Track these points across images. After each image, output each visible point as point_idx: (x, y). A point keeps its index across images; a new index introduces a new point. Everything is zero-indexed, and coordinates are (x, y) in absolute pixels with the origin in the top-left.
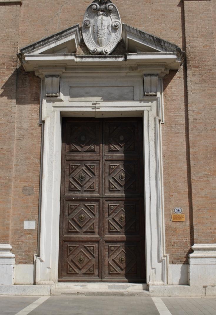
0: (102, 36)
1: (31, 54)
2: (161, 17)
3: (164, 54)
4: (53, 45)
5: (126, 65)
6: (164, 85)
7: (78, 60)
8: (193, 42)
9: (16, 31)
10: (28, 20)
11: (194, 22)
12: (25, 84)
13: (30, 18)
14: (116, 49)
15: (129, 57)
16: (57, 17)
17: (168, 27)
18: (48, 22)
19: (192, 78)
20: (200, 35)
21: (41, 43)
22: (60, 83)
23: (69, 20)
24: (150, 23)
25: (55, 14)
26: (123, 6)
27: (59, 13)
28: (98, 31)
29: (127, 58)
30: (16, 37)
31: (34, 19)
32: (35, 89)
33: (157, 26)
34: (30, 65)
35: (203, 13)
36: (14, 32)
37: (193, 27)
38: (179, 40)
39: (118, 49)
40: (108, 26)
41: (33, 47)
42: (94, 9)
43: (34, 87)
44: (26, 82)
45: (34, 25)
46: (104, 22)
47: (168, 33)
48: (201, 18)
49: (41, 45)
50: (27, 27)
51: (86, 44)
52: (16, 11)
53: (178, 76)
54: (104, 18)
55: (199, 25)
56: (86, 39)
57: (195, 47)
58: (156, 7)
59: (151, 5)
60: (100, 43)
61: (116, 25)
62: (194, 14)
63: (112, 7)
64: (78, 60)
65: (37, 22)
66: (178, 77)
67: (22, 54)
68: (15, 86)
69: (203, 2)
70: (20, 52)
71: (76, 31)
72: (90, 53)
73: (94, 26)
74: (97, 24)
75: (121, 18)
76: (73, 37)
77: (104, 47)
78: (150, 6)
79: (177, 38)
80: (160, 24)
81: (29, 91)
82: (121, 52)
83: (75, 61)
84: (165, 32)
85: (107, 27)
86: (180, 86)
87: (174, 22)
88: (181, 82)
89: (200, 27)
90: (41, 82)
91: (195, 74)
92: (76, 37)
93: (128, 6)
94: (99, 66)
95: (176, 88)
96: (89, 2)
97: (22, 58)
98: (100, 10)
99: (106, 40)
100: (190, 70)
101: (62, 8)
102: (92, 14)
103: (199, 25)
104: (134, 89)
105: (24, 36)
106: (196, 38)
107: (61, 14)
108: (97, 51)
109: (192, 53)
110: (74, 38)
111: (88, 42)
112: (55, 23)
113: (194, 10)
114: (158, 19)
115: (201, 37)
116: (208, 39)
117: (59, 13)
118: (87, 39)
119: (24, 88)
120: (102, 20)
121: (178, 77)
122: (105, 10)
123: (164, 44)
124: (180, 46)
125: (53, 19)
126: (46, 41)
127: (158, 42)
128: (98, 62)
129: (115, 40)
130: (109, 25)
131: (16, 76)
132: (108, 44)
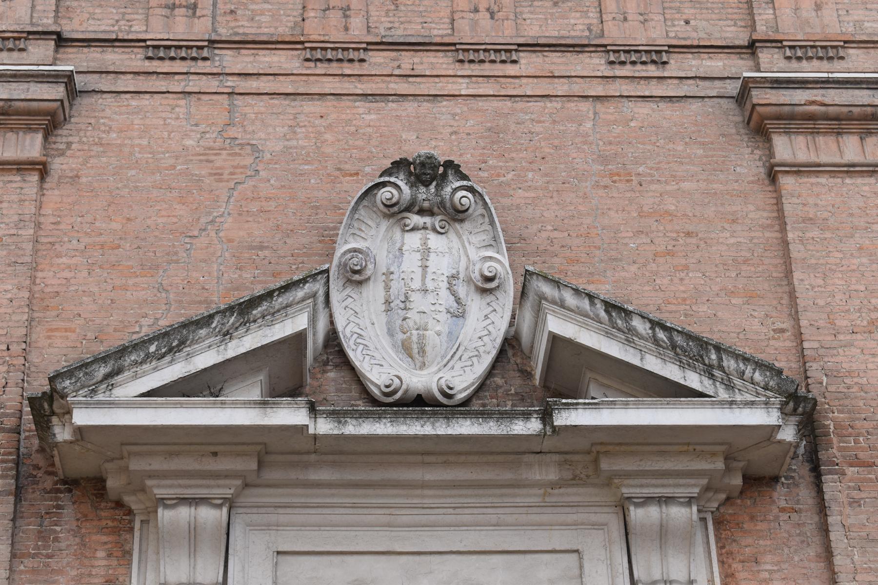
1: (100, 397)
2: (681, 242)
3: (722, 404)
4: (205, 358)
6: (723, 547)
7: (324, 427)
8: (835, 352)
9: (15, 291)
10: (75, 242)
11: (834, 267)
12: (56, 539)
13: (86, 233)
14: (488, 382)
15: (565, 418)
16: (213, 234)
17: (716, 288)
18: (168, 254)
19: (848, 516)
20: (865, 323)
21: (152, 349)
22: (228, 534)
23: (267, 247)
24: (633, 268)
25: (203, 220)
26: (511, 192)
27: (222, 216)
28: (407, 297)
30: (14, 318)
31: (102, 239)
32: (104, 563)
33: (666, 281)
34: (89, 446)
35: (866, 228)
36: (9, 296)
37: (830, 288)
38: (772, 342)
39: (499, 380)
41: (117, 360)
42: (388, 203)
43: (101, 554)
44: (58, 528)
45: (101, 267)
46: (433, 262)
47: (719, 314)
48: (860, 248)
49: (148, 357)
50: (67, 274)
51: (351, 354)
52: (22, 201)
53: (783, 504)
54: (434, 241)
55: (854, 281)
56: (349, 335)
57: (850, 373)
58: (657, 200)
59: (633, 190)
60: (416, 351)
61: (489, 275)
62: (828, 235)
63: (470, 195)
64: (324, 427)
65: (116, 251)
66: (783, 510)
67: (56, 396)
68: (658, 541)
69: (864, 185)
70: (47, 388)
71: (314, 295)
72: (374, 401)
74: (404, 267)
76: (298, 322)
77: (434, 368)
78: (628, 195)
79: (763, 337)
80: (683, 275)
81: (74, 573)
82: (513, 392)
83: (311, 431)
84: (705, 308)
85: (445, 279)
86: (796, 551)
87: (744, 267)
88: (799, 535)
89: (862, 288)
90: (132, 529)
91: (863, 495)
93: (532, 194)
95: (778, 563)
96: (357, 174)
97: (53, 413)
98: (417, 208)
99: (444, 337)
100: (836, 477)
101: (235, 193)
102: (378, 225)
103: (854, 281)
104: (581, 567)
105: (54, 313)
106: (849, 337)
107: (230, 220)
108: (404, 387)
109: (837, 403)
111: (361, 347)
112: (205, 261)
113: (826, 215)
114: (670, 253)
115: (870, 332)
116: (572, 222)
117: (222, 216)
118: (353, 333)
119: (49, 556)
120: (426, 252)
121: (783, 510)
122: (436, 209)
123: (720, 359)
124: (787, 364)
125: (194, 242)
126: (174, 340)
127: (695, 349)
128: (415, 437)
130: (454, 272)
131: (12, 499)
132: (452, 357)
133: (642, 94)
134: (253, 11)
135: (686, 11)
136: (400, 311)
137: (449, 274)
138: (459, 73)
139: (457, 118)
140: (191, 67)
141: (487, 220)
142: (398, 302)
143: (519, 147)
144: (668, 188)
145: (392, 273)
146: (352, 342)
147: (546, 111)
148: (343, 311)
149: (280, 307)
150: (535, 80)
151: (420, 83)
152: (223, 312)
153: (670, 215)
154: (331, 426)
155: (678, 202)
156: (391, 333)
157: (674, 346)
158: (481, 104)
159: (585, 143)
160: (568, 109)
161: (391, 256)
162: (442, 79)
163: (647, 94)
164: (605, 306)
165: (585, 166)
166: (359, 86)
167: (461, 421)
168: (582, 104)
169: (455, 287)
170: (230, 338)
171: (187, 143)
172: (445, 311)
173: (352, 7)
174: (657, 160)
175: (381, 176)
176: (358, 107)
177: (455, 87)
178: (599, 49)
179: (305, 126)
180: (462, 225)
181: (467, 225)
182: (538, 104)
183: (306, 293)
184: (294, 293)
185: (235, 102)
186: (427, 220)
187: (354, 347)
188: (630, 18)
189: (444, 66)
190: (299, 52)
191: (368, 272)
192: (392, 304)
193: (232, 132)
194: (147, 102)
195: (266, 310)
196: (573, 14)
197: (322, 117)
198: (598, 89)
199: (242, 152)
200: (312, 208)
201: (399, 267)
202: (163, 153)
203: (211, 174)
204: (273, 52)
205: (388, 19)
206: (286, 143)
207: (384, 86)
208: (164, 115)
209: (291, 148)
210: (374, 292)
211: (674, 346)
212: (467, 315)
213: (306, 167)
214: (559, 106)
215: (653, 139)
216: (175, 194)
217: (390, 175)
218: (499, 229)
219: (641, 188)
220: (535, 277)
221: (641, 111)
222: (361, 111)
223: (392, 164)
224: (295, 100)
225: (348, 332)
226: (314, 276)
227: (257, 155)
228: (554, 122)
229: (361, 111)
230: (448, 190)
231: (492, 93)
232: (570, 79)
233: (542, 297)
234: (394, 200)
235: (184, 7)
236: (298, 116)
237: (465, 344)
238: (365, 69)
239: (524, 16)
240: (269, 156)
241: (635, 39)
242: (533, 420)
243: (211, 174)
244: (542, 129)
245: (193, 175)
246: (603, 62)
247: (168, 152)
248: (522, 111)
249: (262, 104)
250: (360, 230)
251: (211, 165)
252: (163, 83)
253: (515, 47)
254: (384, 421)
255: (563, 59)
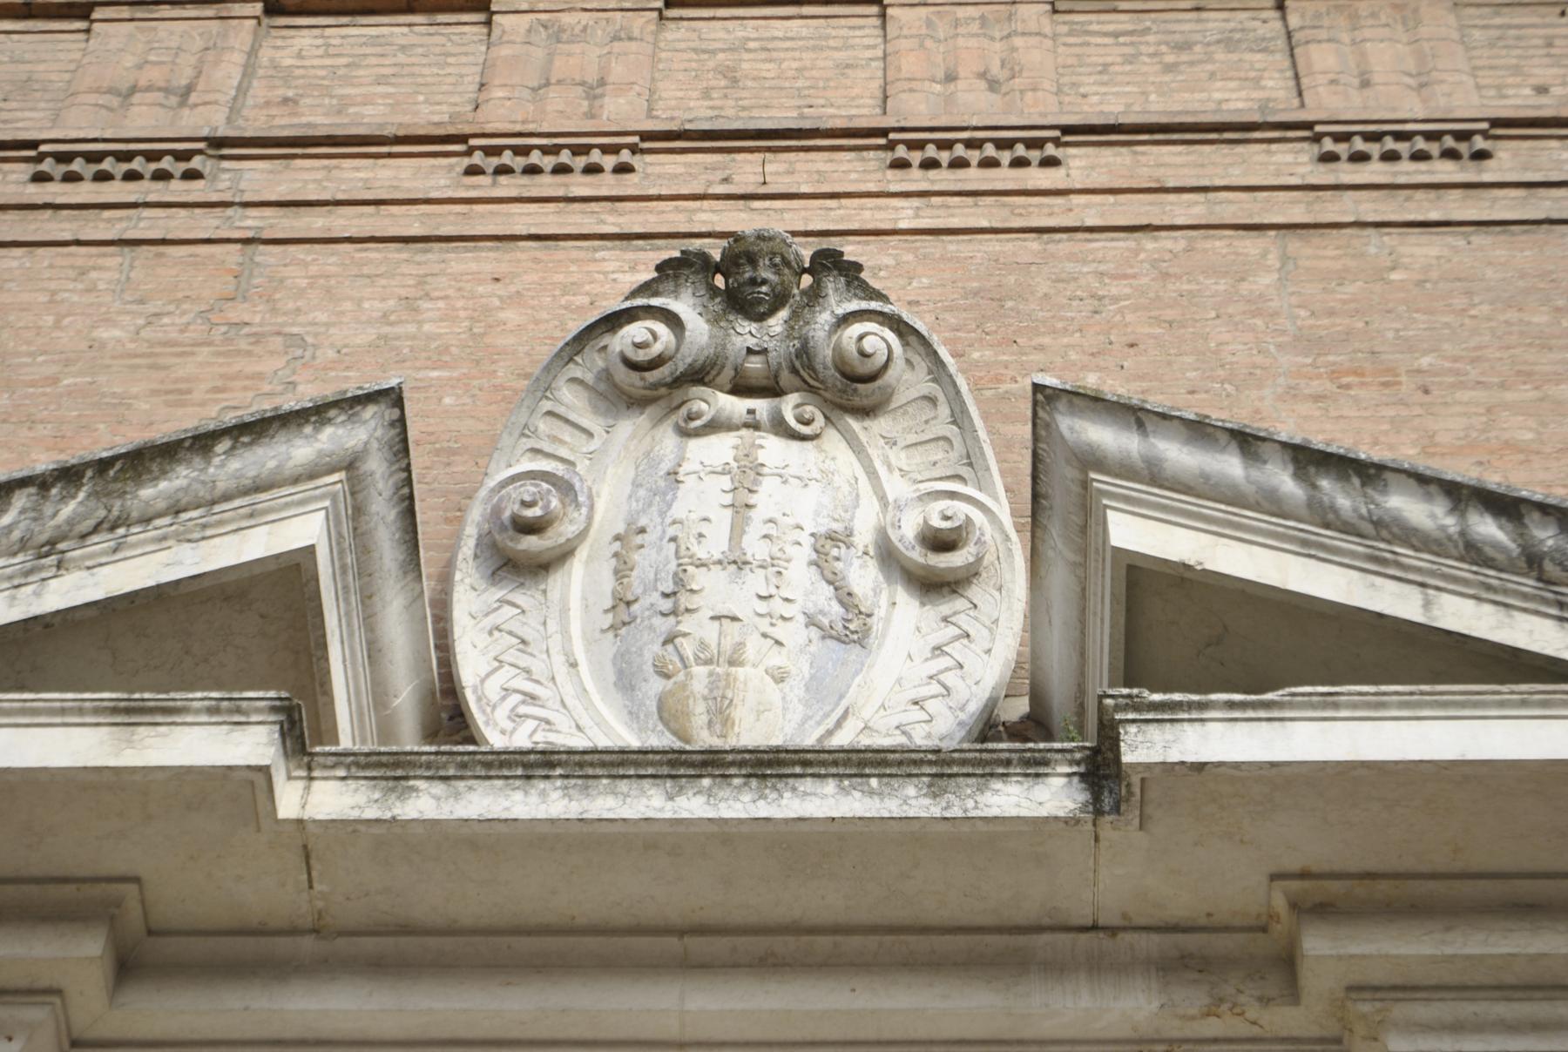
0: (741, 645)
5: (1113, 931)
29: (1127, 758)
40: (832, 537)
42: (641, 356)
46: (769, 496)
59: (1403, 403)
71: (351, 465)
73: (628, 538)
74: (678, 511)
75: (1002, 473)
85: (808, 542)
92: (335, 537)
94: (673, 941)
99: (795, 689)
110: (310, 550)
120: (747, 475)
122: (786, 378)
129: (931, 706)
133: (1420, 218)
134: (342, 97)
135: (1536, 71)
136: (658, 621)
137: (822, 530)
138: (894, 188)
139: (882, 274)
140: (147, 193)
141: (944, 411)
142: (655, 597)
143: (1060, 325)
144: (1509, 396)
145: (642, 531)
146: (501, 715)
147: (1142, 256)
148: (483, 640)
149: (232, 484)
150: (1111, 198)
151: (782, 210)
152: (41, 483)
153: (1521, 451)
154: (361, 798)
155: (1544, 424)
156: (625, 682)
157: (1533, 561)
158: (952, 245)
159: (1256, 314)
160: (1205, 251)
161: (642, 492)
162: (844, 201)
163: (1434, 216)
164: (1295, 460)
165: (1259, 359)
166: (611, 219)
167: (807, 785)
168: (1248, 243)
169: (839, 565)
170: (59, 566)
171: (105, 335)
172: (801, 619)
173: (611, 79)
174: (1472, 343)
175: (627, 299)
176: (604, 260)
177: (879, 215)
178: (1291, 134)
179: (446, 298)
180: (867, 423)
181: (881, 425)
182: (1121, 244)
183: (321, 454)
184: (283, 448)
185: (258, 259)
186: (761, 406)
187: (509, 725)
188: (1376, 78)
189: (853, 176)
190: (453, 160)
191: (565, 530)
192: (635, 608)
193: (236, 313)
194: (15, 264)
195: (185, 490)
196: (1219, 84)
197: (497, 280)
198: (1295, 209)
199: (257, 349)
200: (438, 452)
201: (662, 514)
202: (30, 354)
203: (155, 393)
204: (381, 162)
205: (711, 103)
206: (386, 330)
207: (681, 217)
208: (53, 285)
209: (398, 338)
210: (581, 585)
211: (1533, 561)
212: (872, 641)
213: (435, 374)
214: (1182, 244)
215: (1459, 302)
216: (42, 431)
217: (656, 294)
218: (982, 434)
219: (1427, 399)
220: (1062, 405)
221: (1417, 251)
222: (610, 266)
223: (659, 268)
224: (426, 251)
225: (492, 689)
226: (352, 403)
227: (299, 352)
228: (1166, 276)
229: (610, 266)
230: (824, 318)
231: (985, 224)
232: (1211, 195)
233: (1091, 460)
234: (657, 348)
235: (159, 89)
236: (429, 279)
237: (867, 713)
238: (629, 185)
239: (1082, 90)
240: (331, 354)
241: (1394, 109)
242: (1057, 782)
243: (155, 393)
244: (1128, 291)
245: (104, 395)
246: (1304, 158)
247: (45, 353)
248: (1071, 257)
249: (333, 259)
250: (555, 439)
251: (162, 374)
252: (67, 225)
253: (1057, 133)
254: (542, 784)
255: (1191, 158)
